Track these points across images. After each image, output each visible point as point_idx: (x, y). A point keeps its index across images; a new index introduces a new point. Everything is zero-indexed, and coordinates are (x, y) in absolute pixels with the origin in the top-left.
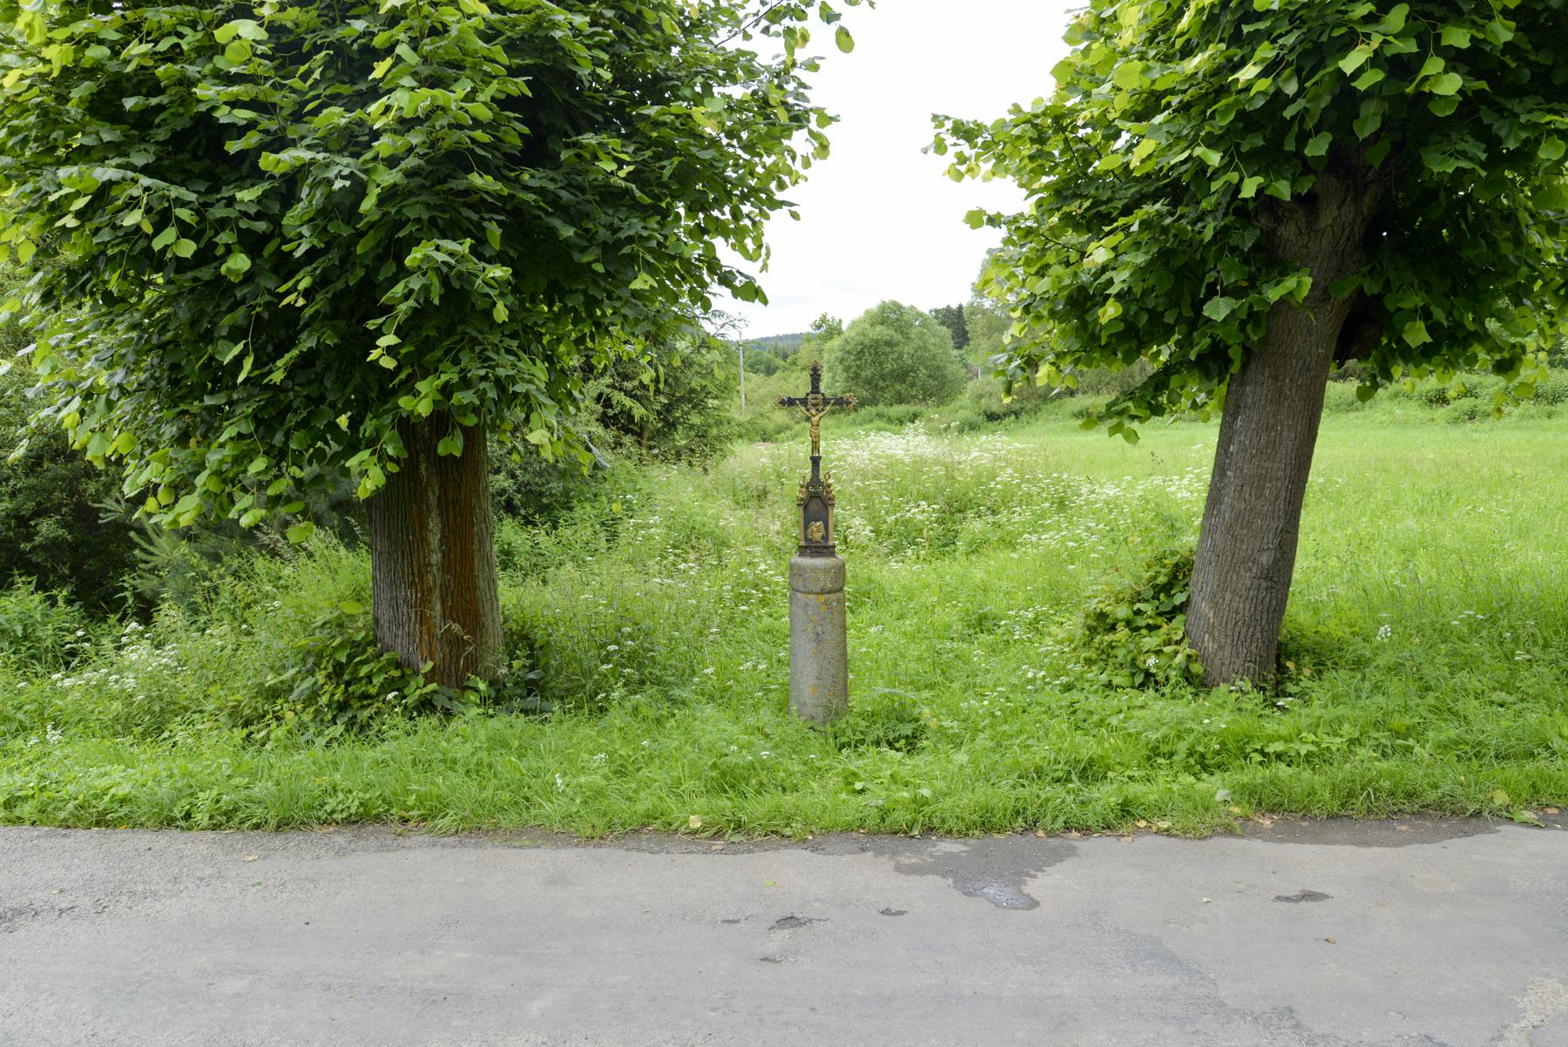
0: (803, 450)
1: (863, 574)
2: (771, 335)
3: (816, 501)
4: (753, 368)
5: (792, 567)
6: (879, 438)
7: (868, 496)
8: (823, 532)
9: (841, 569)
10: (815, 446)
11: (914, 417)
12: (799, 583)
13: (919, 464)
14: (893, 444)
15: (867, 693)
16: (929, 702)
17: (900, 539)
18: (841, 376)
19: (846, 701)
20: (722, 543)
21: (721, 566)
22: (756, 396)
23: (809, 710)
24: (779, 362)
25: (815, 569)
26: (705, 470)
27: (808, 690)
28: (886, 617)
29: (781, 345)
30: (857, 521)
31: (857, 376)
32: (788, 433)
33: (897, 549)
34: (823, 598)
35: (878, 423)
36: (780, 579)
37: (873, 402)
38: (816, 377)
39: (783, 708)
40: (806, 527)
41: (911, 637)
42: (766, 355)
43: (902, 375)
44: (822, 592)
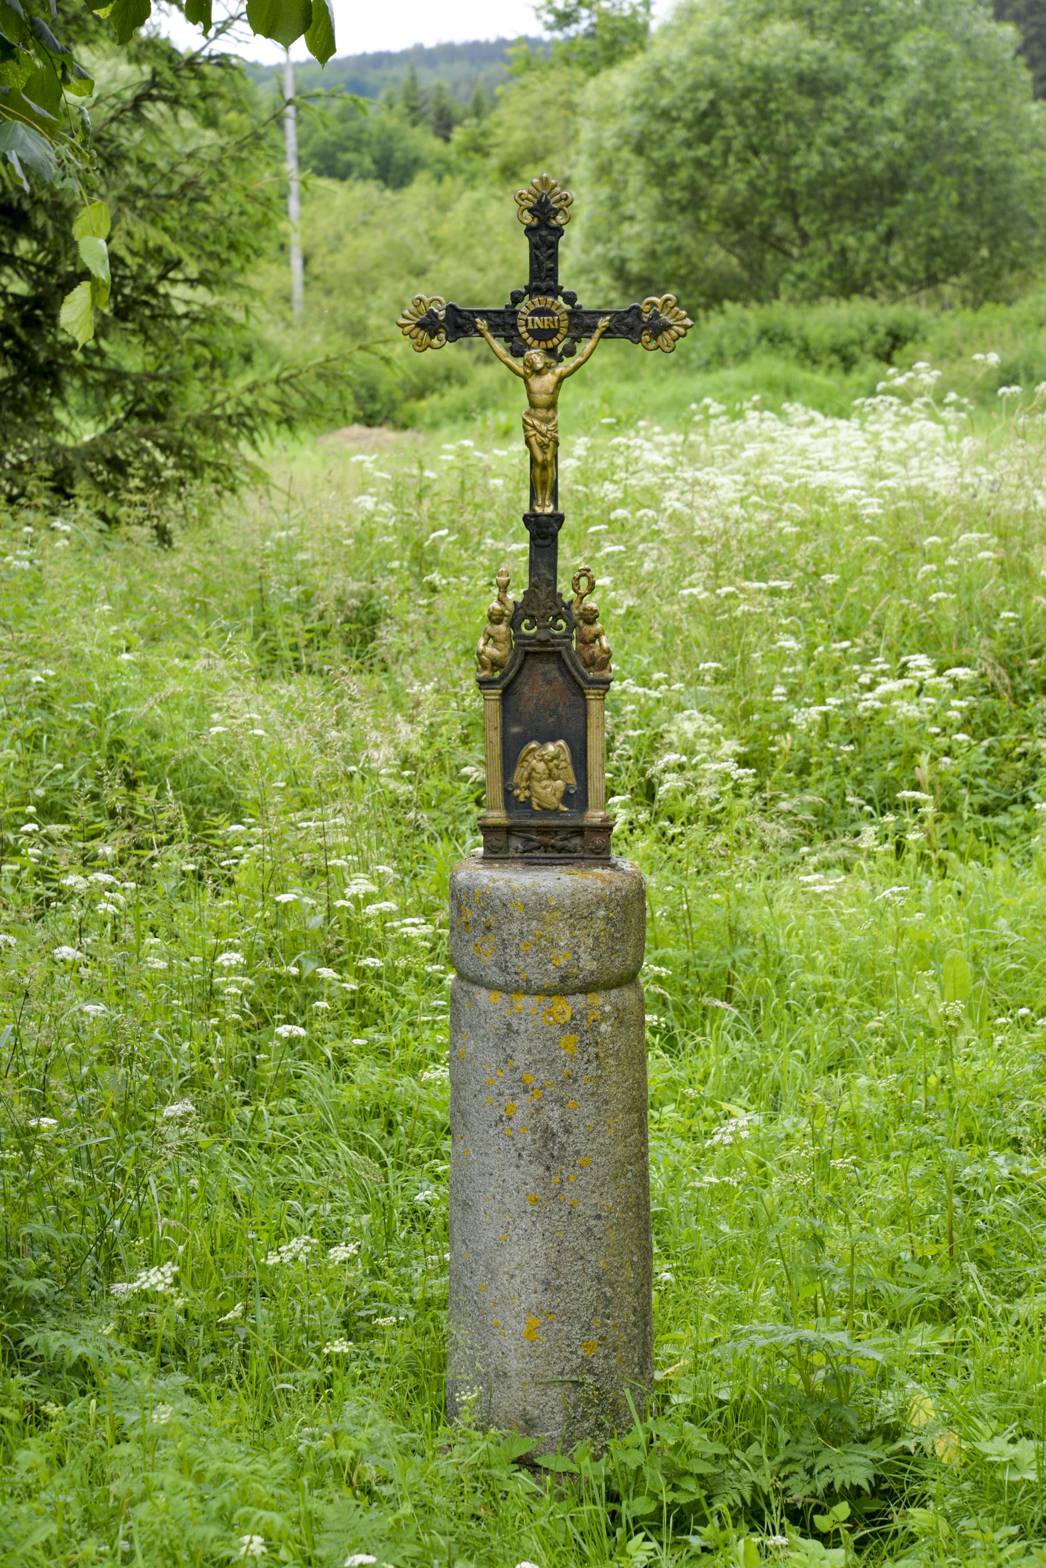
0: (503, 463)
1: (711, 906)
2: (396, 46)
3: (545, 668)
4: (329, 163)
5: (459, 896)
6: (770, 424)
7: (728, 634)
8: (568, 776)
9: (632, 904)
10: (543, 476)
11: (893, 345)
12: (485, 957)
13: (911, 524)
14: (823, 449)
15: (718, 1341)
16: (936, 1372)
17: (846, 787)
18: (642, 200)
19: (645, 1363)
20: (211, 802)
21: (209, 876)
22: (342, 262)
23: (511, 1399)
24: (423, 141)
25: (539, 907)
26: (163, 536)
27: (515, 1336)
28: (786, 1064)
29: (429, 80)
30: (689, 724)
31: (696, 199)
32: (454, 395)
33: (825, 824)
34: (565, 1007)
35: (769, 365)
36: (416, 928)
37: (754, 287)
38: (544, 225)
39: (426, 1392)
40: (510, 756)
41: (869, 1136)
42: (379, 116)
43: (864, 195)
44: (566, 986)
